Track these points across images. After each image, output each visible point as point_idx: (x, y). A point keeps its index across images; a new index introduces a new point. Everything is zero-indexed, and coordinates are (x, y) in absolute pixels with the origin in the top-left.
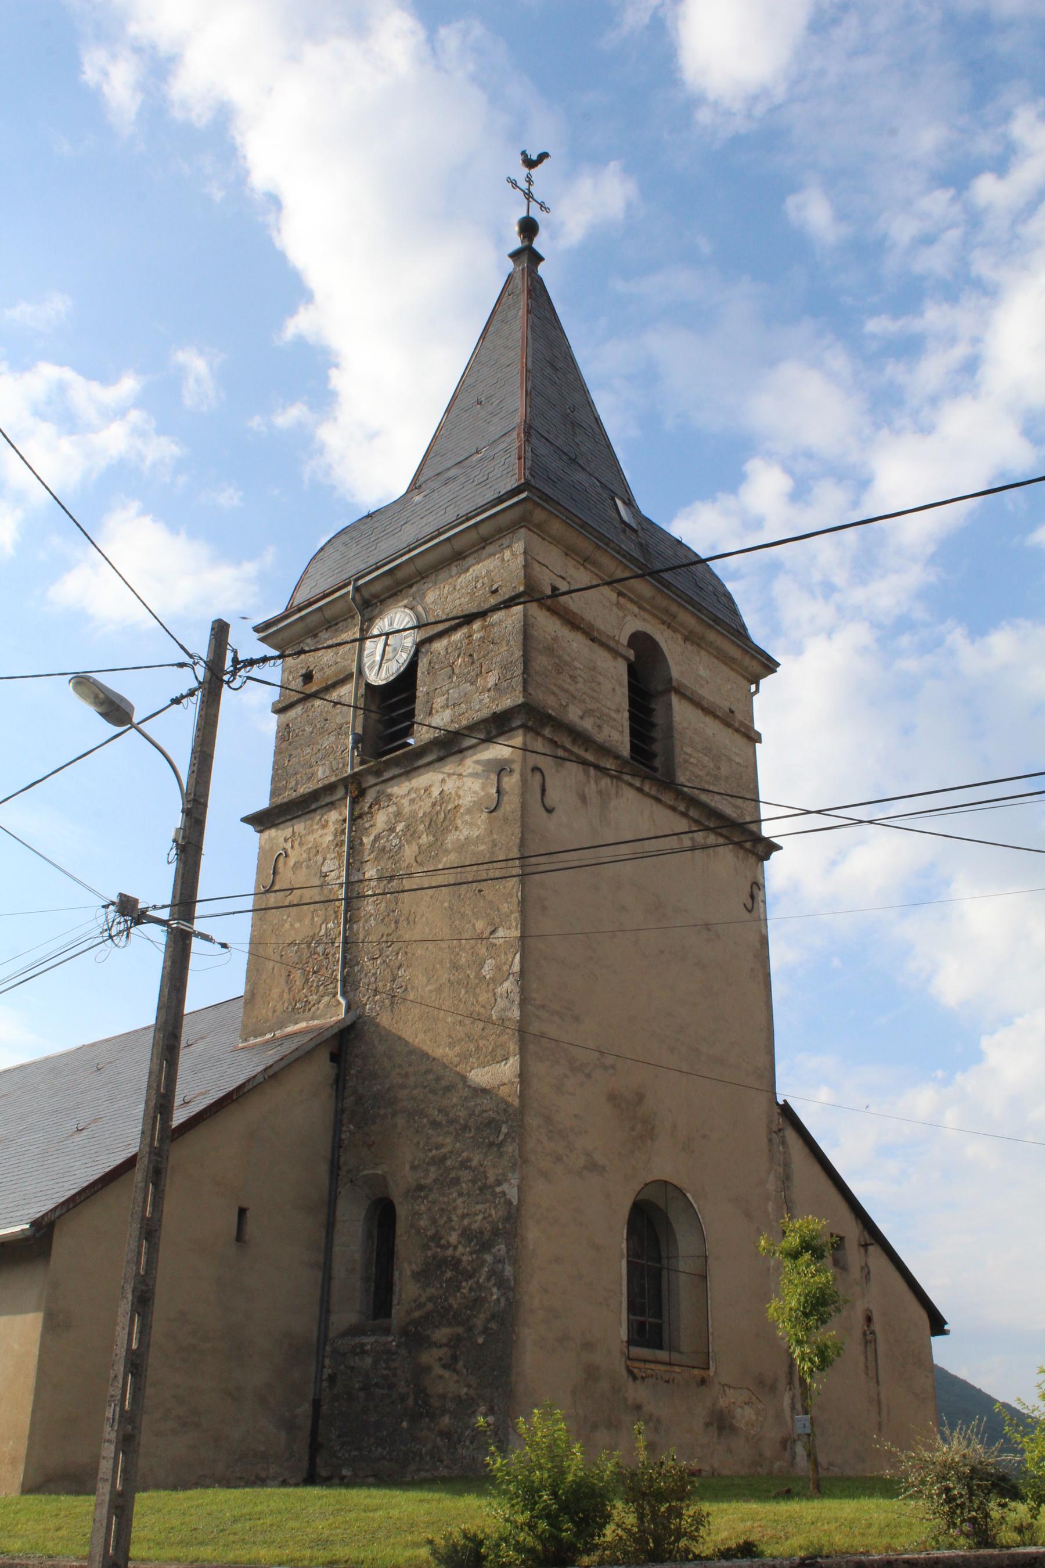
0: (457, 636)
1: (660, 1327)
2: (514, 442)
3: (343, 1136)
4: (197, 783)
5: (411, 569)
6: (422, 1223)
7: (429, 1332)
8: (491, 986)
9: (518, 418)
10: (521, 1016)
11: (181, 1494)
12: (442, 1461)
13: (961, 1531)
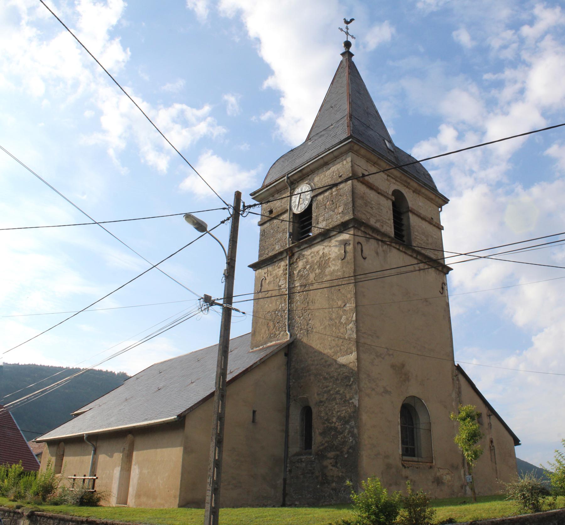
0: (327, 194)
1: (414, 449)
2: (346, 121)
3: (291, 384)
4: (232, 252)
5: (308, 169)
6: (322, 415)
9: (347, 112)
10: (357, 336)
11: (236, 510)
12: (333, 498)
13: (529, 508)
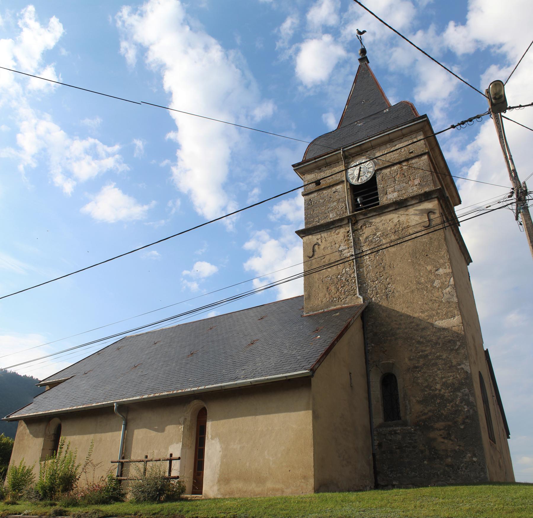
0: (395, 167)
7: (432, 424)
8: (440, 290)
